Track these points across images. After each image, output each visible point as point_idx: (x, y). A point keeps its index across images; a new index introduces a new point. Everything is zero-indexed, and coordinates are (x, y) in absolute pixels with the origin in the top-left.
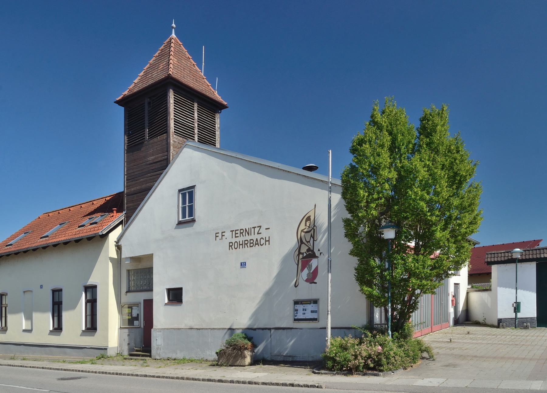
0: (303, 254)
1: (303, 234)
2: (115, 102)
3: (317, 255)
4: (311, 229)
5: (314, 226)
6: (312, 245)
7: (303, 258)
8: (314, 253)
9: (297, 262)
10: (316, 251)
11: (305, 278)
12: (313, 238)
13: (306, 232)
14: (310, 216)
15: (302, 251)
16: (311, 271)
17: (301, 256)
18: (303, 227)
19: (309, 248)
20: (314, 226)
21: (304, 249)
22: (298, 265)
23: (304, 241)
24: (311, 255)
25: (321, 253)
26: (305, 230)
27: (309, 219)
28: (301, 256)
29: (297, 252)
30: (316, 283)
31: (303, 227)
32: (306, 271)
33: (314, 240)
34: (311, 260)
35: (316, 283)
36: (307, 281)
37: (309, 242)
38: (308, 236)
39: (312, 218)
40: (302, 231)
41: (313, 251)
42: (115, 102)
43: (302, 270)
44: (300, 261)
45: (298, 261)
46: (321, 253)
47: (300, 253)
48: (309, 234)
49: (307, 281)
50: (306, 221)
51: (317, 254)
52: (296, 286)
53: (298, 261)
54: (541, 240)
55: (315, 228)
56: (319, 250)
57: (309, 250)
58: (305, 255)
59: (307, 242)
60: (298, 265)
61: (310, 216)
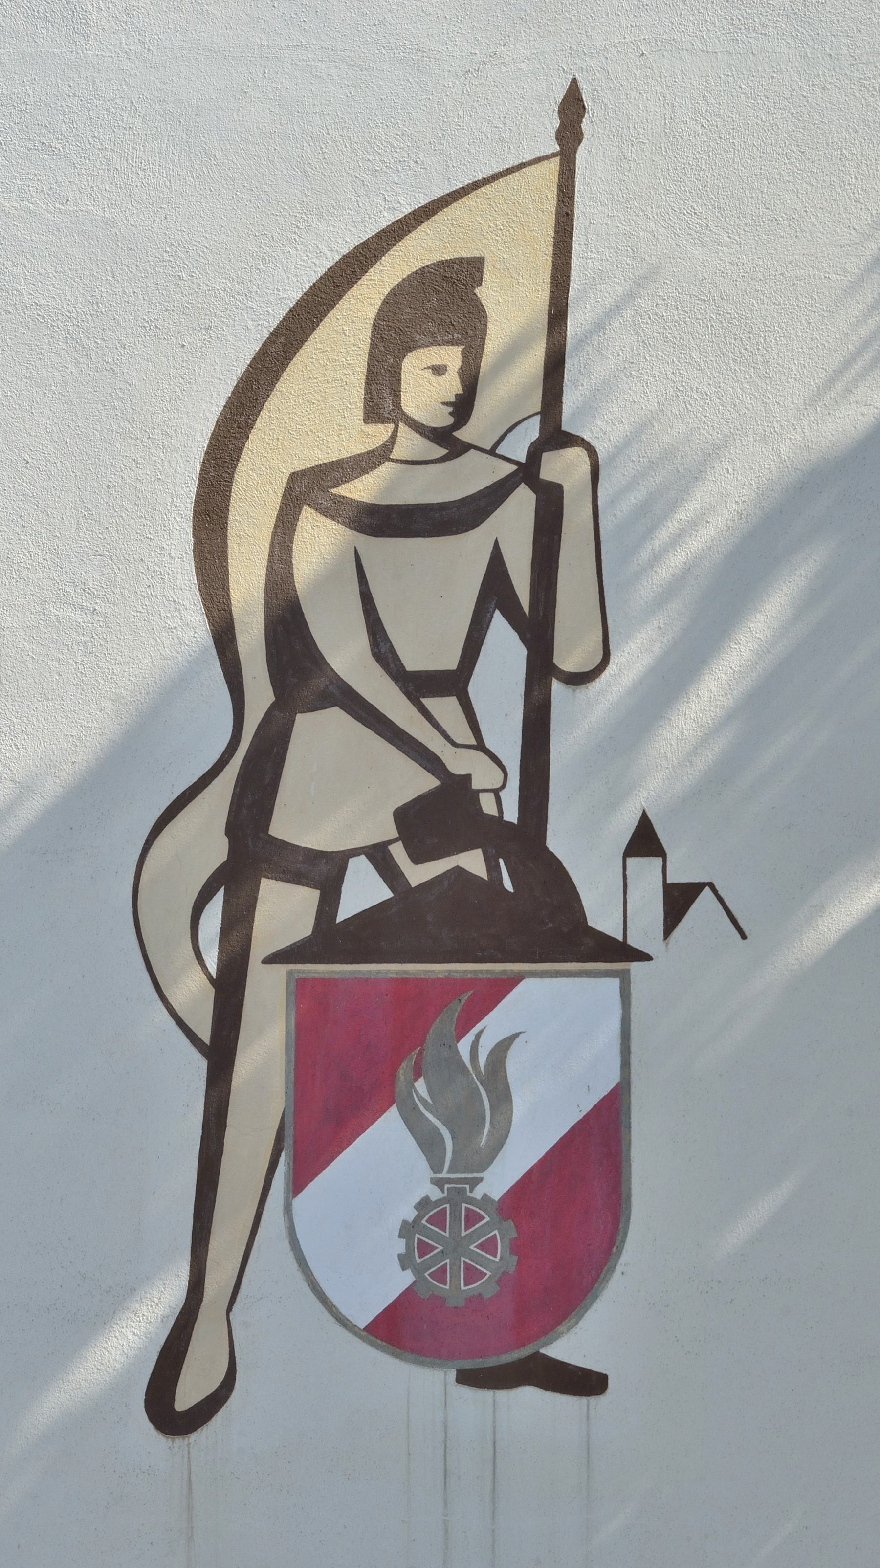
0: (323, 872)
1: (320, 541)
2: (574, 81)
3: (603, 919)
4: (472, 476)
5: (554, 437)
6: (506, 736)
7: (331, 939)
8: (554, 885)
9: (194, 992)
10: (583, 843)
11: (378, 1282)
12: (537, 633)
13: (384, 521)
14: (469, 271)
15: (293, 822)
16: (499, 1180)
17: (284, 911)
18: (319, 414)
19: (455, 792)
20: (554, 437)
21: (342, 792)
22: (220, 1053)
23: (344, 652)
24: (500, 900)
25: (678, 900)
26: (362, 490)
27: (445, 301)
28: (284, 911)
29: (202, 840)
30: (586, 1383)
31: (319, 414)
32: (387, 1162)
33: (541, 669)
34: (496, 991)
35: (586, 1383)
36: (397, 1329)
37: (454, 683)
38: (432, 596)
39: (511, 305)
40: (308, 488)
41: (524, 841)
42: (574, 81)
43: (312, 1140)
44: (268, 993)
45: (229, 987)
46: (678, 900)
47: (252, 853)
48: (461, 560)
49: (397, 1329)
50: (391, 341)
51: (609, 894)
52: (168, 1413)
53: (229, 987)
54: (496, 543)
55: (564, 468)
56: (645, 841)
57: (440, 816)
58: (363, 891)
59: (419, 686)
60: (220, 1053)
61: (469, 271)
